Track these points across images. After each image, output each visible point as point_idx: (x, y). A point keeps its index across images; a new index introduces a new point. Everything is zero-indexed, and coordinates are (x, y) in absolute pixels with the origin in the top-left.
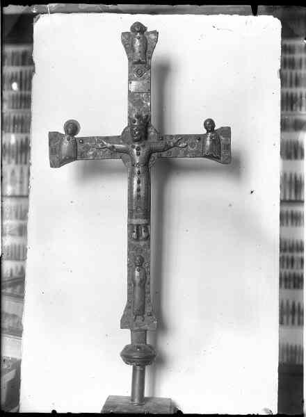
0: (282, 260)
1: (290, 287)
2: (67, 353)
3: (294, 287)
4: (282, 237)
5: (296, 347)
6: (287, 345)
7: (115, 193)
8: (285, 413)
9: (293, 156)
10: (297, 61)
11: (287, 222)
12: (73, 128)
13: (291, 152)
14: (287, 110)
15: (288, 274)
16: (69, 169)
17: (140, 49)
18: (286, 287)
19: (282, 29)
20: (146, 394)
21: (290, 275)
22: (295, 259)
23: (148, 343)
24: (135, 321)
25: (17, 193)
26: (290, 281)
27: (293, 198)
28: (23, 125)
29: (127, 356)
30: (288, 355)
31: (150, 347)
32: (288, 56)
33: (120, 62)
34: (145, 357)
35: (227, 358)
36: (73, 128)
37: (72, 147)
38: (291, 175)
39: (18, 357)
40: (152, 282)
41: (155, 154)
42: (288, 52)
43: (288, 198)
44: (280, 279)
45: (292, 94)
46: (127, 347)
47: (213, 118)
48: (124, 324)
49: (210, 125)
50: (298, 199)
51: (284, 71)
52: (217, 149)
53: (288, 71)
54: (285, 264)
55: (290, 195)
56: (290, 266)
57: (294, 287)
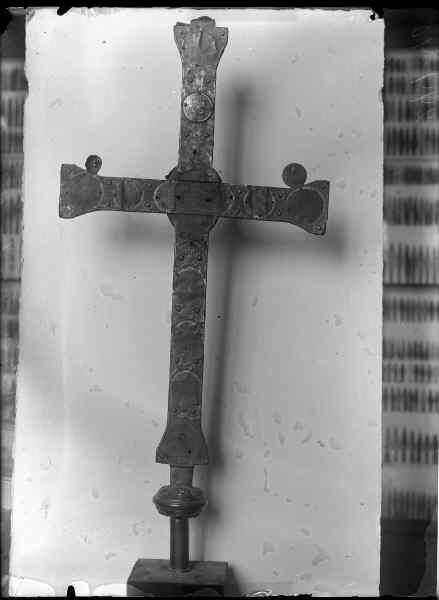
0: (386, 370)
1: (399, 409)
3: (405, 409)
4: (387, 339)
6: (395, 494)
7: (153, 276)
8: (391, 594)
9: (403, 220)
11: (395, 314)
12: (94, 162)
13: (403, 213)
14: (394, 153)
15: (396, 392)
16: (93, 221)
18: (393, 409)
19: (386, 30)
20: (192, 557)
21: (399, 390)
22: (406, 367)
23: (194, 485)
24: (46, 517)
25: (403, 280)
28: (405, 267)
29: (163, 503)
30: (395, 506)
31: (199, 492)
32: (396, 75)
34: (188, 506)
35: (318, 495)
36: (94, 162)
37: (84, 189)
41: (213, 210)
43: (395, 280)
44: (385, 397)
45: (401, 131)
46: (163, 490)
48: (162, 456)
49: (295, 173)
50: (424, 281)
51: (388, 97)
52: (304, 203)
53: (396, 98)
54: (392, 376)
55: (421, 278)
56: (399, 378)
57: (405, 409)
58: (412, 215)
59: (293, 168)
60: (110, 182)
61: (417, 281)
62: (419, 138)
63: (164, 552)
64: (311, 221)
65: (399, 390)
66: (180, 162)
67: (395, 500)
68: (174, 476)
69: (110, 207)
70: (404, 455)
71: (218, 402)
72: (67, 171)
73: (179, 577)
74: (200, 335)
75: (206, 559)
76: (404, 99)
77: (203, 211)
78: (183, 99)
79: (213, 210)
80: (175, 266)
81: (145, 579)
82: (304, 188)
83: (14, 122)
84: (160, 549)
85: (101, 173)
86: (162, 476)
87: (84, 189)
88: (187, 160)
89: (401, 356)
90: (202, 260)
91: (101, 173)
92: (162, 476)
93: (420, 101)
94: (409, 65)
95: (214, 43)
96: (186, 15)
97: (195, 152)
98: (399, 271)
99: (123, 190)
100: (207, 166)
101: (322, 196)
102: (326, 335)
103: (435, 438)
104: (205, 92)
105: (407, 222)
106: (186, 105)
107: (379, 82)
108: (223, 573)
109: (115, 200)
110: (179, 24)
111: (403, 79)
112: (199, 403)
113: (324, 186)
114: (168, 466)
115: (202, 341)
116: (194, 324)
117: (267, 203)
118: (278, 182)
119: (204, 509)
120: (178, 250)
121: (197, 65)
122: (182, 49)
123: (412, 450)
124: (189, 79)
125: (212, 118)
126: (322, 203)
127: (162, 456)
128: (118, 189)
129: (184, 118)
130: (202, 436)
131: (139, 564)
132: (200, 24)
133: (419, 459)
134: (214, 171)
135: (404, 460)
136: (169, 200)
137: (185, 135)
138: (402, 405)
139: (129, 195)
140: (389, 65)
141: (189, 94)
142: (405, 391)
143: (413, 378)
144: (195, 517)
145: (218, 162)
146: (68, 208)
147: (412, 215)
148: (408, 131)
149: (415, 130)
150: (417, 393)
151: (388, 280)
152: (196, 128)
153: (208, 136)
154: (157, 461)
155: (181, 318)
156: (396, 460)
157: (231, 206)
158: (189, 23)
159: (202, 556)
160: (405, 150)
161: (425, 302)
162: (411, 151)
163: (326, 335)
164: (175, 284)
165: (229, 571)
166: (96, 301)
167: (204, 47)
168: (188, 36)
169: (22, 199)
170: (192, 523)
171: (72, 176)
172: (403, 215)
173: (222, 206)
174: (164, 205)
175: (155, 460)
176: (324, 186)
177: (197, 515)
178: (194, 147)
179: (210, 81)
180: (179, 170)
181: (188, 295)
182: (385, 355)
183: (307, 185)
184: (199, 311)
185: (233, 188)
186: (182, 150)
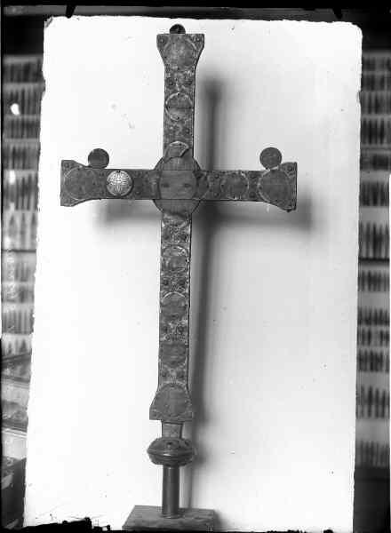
9: (371, 202)
12: (99, 157)
13: (371, 196)
16: (88, 210)
20: (182, 504)
23: (183, 437)
29: (156, 453)
34: (180, 455)
36: (99, 157)
37: (87, 180)
41: (199, 196)
45: (370, 122)
48: (153, 416)
49: (270, 156)
50: (377, 256)
52: (278, 187)
57: (372, 369)
58: (379, 201)
63: (155, 499)
65: (366, 353)
70: (370, 411)
73: (170, 522)
76: (373, 94)
83: (20, 206)
86: (155, 430)
87: (87, 180)
92: (155, 430)
93: (28, 119)
94: (378, 64)
96: (164, 25)
98: (368, 247)
102: (292, 302)
105: (375, 203)
111: (373, 77)
113: (293, 168)
114: (159, 422)
117: (249, 186)
123: (377, 407)
127: (153, 416)
135: (369, 414)
138: (368, 366)
140: (367, 65)
142: (372, 353)
143: (379, 342)
144: (184, 465)
148: (376, 122)
149: (383, 122)
150: (382, 356)
151: (364, 255)
160: (373, 140)
161: (376, 273)
162: (379, 141)
163: (292, 302)
166: (93, 289)
169: (34, 316)
170: (182, 470)
172: (371, 197)
176: (293, 168)
179: (190, 82)
182: (360, 322)
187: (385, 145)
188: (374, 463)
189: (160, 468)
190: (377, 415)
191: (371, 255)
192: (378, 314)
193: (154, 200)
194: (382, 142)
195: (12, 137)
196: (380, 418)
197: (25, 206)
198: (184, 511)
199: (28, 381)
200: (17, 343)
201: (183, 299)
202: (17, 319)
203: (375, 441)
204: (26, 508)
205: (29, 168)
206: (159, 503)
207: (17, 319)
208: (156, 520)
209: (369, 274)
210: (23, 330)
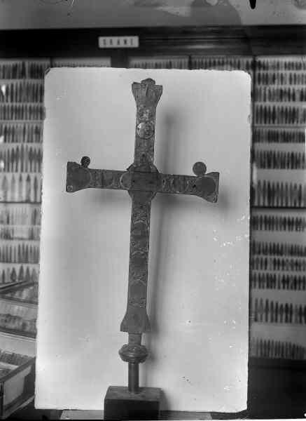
1: (263, 287)
2: (69, 369)
3: (268, 287)
5: (271, 152)
7: (117, 222)
10: (270, 77)
12: (86, 160)
17: (148, 95)
20: (140, 385)
26: (264, 281)
27: (266, 204)
29: (124, 355)
33: (129, 106)
35: (210, 364)
36: (86, 160)
37: (80, 175)
38: (265, 182)
39: (31, 355)
40: (151, 235)
42: (262, 68)
46: (125, 347)
47: (203, 161)
48: (123, 328)
49: (200, 167)
50: (271, 205)
52: (205, 185)
56: (264, 267)
57: (268, 287)
58: (272, 164)
59: (199, 165)
60: (95, 172)
61: (275, 205)
62: (277, 113)
63: (125, 383)
64: (208, 195)
66: (136, 162)
67: (261, 345)
68: (131, 340)
69: (95, 186)
71: (155, 296)
72: (71, 166)
73: (133, 396)
74: (145, 260)
75: (149, 386)
77: (148, 189)
78: (137, 125)
79: (155, 185)
80: (132, 219)
81: (114, 398)
82: (206, 176)
84: (120, 377)
85: (90, 167)
86: (125, 338)
88: (139, 160)
89: (265, 252)
90: (147, 217)
91: (90, 167)
92: (125, 338)
95: (154, 94)
97: (143, 155)
99: (103, 177)
100: (151, 164)
101: (215, 180)
103: (304, 278)
104: (149, 121)
106: (139, 129)
107: (248, 111)
108: (159, 394)
109: (97, 182)
110: (135, 83)
112: (145, 298)
113: (216, 175)
115: (147, 262)
116: (142, 253)
117: (181, 184)
118: (190, 173)
119: (148, 357)
120: (133, 210)
121: (145, 107)
122: (136, 97)
124: (140, 114)
125: (153, 136)
126: (215, 185)
127: (123, 328)
128: (100, 176)
129: (137, 136)
130: (147, 316)
131: (111, 389)
132: (146, 83)
133: (276, 320)
134: (154, 166)
135: (267, 320)
136: (129, 182)
137: (138, 146)
139: (106, 180)
141: (140, 122)
145: (156, 161)
146: (72, 187)
147: (272, 164)
152: (144, 141)
153: (150, 149)
154: (69, 163)
155: (135, 249)
156: (261, 319)
157: (163, 187)
158: (140, 82)
159: (146, 384)
162: (271, 121)
163: (212, 261)
164: (132, 230)
165: (162, 393)
167: (149, 96)
168: (139, 90)
170: (140, 365)
171: (73, 168)
173: (159, 185)
174: (126, 186)
175: (70, 161)
176: (216, 175)
177: (144, 361)
178: (143, 153)
179: (152, 116)
180: (135, 166)
181: (140, 235)
183: (208, 174)
184: (146, 245)
185: (166, 176)
186: (136, 153)
187: (276, 125)
188: (270, 356)
189: (127, 364)
190: (272, 321)
191: (266, 204)
192: (284, 110)
193: (52, 67)
194: (274, 123)
195: (5, 119)
196: (274, 323)
197: (14, 169)
198: (142, 388)
199: (37, 304)
200: (8, 270)
201: (143, 255)
202: (9, 252)
203: (284, 243)
204: (36, 389)
205: (17, 141)
206: (127, 385)
207: (9, 252)
208: (126, 396)
209: (266, 217)
210: (13, 260)
